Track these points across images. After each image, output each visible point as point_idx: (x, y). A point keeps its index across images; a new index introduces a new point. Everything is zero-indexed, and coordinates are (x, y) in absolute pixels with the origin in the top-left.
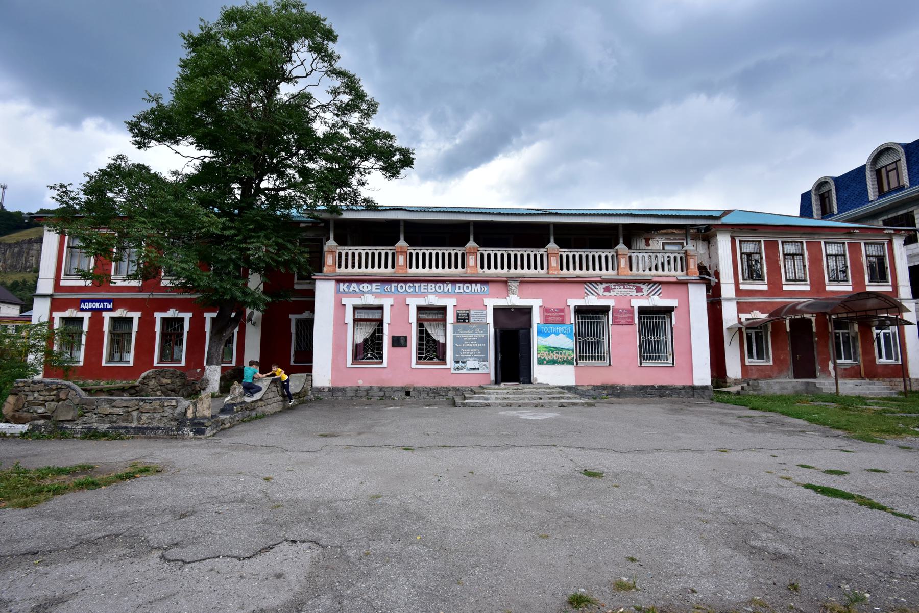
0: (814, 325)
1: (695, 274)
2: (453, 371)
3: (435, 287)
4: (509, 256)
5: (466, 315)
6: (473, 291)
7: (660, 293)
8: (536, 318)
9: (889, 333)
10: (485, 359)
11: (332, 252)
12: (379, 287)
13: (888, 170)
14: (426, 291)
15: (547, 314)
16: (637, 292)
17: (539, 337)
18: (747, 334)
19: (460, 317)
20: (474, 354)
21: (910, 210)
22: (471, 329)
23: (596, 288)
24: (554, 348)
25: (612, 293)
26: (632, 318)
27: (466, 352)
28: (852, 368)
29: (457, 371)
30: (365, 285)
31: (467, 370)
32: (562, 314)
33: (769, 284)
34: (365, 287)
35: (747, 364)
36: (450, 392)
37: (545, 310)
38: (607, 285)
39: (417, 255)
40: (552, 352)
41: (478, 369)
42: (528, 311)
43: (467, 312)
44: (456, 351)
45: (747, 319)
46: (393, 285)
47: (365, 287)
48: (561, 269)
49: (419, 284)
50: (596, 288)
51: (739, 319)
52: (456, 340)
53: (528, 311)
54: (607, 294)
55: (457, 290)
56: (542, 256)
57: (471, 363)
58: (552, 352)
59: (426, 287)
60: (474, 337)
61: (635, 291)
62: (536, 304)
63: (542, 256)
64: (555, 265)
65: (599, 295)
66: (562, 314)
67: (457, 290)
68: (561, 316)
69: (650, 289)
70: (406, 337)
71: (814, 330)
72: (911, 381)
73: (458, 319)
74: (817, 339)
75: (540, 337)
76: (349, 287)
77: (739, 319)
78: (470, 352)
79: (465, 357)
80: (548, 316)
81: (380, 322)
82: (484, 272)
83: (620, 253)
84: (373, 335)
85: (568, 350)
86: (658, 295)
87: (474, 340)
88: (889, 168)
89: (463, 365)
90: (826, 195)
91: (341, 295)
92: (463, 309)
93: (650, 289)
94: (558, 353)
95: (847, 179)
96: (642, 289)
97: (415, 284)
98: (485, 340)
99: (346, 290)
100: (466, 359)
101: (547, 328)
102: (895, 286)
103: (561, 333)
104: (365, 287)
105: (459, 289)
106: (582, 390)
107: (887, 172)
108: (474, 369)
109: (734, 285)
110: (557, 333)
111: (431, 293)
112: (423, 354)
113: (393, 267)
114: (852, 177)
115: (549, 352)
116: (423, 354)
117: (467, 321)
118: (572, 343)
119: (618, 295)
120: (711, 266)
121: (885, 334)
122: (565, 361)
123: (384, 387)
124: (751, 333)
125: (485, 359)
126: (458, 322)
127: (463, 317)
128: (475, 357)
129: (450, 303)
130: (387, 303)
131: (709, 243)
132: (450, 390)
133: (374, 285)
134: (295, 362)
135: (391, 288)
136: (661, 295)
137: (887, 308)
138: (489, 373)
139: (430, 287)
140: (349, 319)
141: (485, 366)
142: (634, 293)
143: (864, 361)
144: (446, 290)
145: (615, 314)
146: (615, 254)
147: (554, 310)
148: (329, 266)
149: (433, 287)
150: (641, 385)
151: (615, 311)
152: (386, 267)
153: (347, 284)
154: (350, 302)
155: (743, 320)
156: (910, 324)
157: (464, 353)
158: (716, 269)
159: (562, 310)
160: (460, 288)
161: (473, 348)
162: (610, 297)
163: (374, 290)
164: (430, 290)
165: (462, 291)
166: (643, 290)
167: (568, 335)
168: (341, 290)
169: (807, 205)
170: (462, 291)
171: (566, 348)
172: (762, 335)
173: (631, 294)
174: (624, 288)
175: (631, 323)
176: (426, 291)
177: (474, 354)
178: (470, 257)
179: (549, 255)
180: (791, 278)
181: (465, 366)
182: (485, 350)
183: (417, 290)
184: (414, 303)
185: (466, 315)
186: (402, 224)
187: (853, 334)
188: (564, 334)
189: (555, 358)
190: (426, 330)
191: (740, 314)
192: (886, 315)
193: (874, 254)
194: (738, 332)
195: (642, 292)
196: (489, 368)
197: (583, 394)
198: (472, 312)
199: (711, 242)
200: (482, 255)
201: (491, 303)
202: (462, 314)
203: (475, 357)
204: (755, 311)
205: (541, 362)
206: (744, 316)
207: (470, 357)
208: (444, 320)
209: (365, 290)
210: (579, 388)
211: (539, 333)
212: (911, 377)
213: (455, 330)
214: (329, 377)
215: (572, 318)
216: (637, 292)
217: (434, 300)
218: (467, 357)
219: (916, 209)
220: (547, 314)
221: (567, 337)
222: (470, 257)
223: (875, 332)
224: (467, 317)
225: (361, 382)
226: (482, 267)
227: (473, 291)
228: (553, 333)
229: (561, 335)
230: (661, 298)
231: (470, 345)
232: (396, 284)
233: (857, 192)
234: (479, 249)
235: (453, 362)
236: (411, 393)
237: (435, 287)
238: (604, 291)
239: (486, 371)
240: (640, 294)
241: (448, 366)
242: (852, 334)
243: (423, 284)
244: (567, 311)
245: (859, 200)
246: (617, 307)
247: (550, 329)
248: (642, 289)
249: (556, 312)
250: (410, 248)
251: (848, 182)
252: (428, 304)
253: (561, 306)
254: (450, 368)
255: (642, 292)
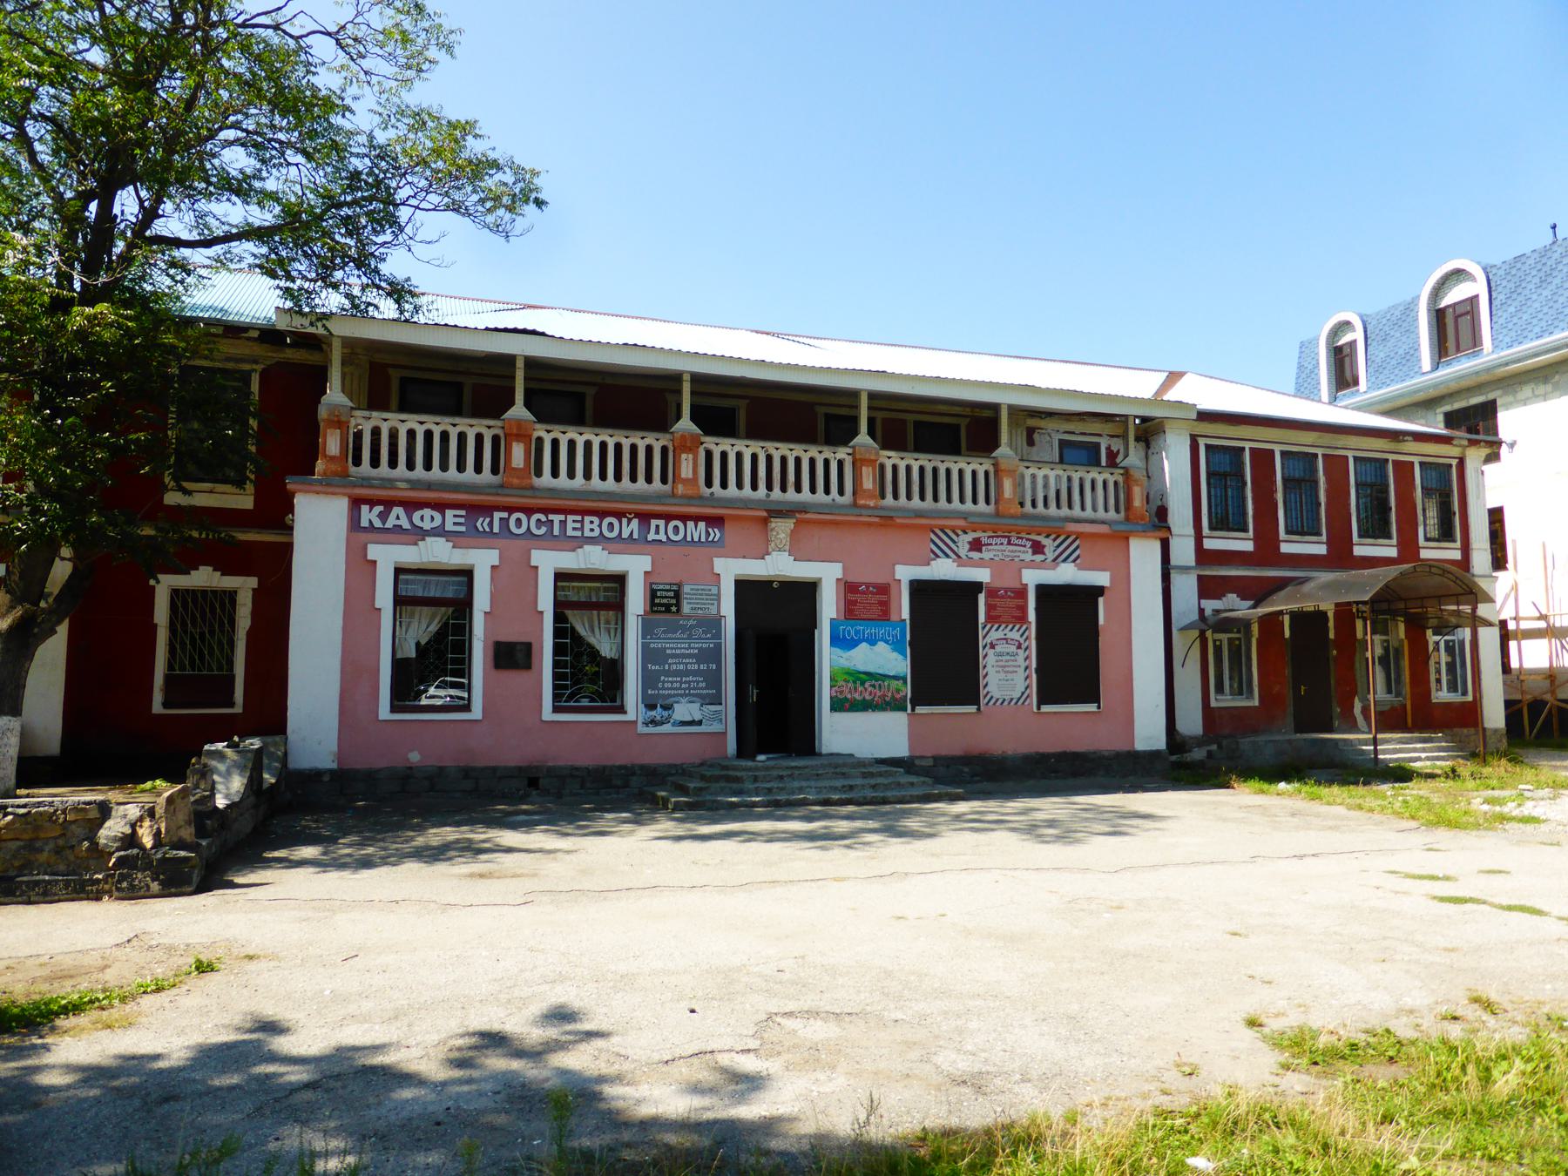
0: (1331, 624)
1: (1142, 519)
2: (641, 729)
3: (600, 526)
4: (769, 458)
5: (672, 594)
6: (689, 539)
7: (1078, 557)
8: (829, 606)
9: (1453, 641)
10: (716, 700)
11: (340, 424)
12: (462, 520)
13: (1458, 313)
14: (579, 534)
15: (851, 597)
16: (1034, 553)
17: (833, 649)
18: (1215, 641)
19: (657, 601)
20: (689, 688)
21: (1491, 396)
22: (684, 629)
23: (954, 542)
24: (865, 673)
25: (986, 555)
26: (1023, 609)
27: (672, 682)
28: (1393, 709)
29: (652, 729)
30: (427, 512)
31: (673, 725)
32: (883, 598)
33: (1256, 539)
34: (427, 518)
35: (1213, 704)
36: (634, 778)
37: (849, 589)
38: (976, 535)
39: (555, 443)
40: (863, 683)
41: (700, 723)
42: (808, 590)
43: (675, 588)
44: (649, 680)
45: (1217, 611)
46: (497, 515)
47: (427, 518)
48: (883, 496)
49: (562, 517)
50: (954, 542)
51: (1201, 611)
52: (648, 655)
53: (808, 590)
54: (975, 555)
55: (651, 536)
56: (841, 463)
57: (684, 711)
58: (863, 683)
59: (578, 525)
60: (689, 648)
61: (1030, 550)
62: (828, 575)
63: (841, 463)
64: (871, 486)
65: (959, 557)
66: (883, 598)
67: (651, 536)
68: (881, 603)
69: (1058, 546)
70: (528, 646)
71: (1332, 635)
72: (1488, 733)
73: (653, 604)
74: (1335, 652)
75: (838, 651)
76: (383, 516)
77: (1201, 611)
78: (681, 682)
79: (670, 696)
80: (855, 603)
81: (463, 606)
82: (712, 494)
83: (1003, 467)
84: (440, 636)
85: (896, 678)
86: (1074, 561)
87: (689, 656)
88: (1460, 310)
89: (666, 714)
90: (1346, 351)
91: (363, 537)
92: (666, 578)
93: (1058, 546)
94: (874, 686)
95: (1384, 321)
96: (1044, 546)
97: (551, 517)
98: (716, 654)
99: (378, 523)
100: (672, 699)
101: (851, 629)
102: (1466, 549)
103: (882, 640)
104: (427, 518)
105: (657, 532)
106: (921, 766)
107: (1456, 318)
108: (692, 723)
109: (1193, 539)
110: (872, 642)
111: (591, 541)
112: (565, 687)
113: (495, 470)
114: (1394, 318)
115: (854, 682)
116: (565, 687)
117: (674, 609)
118: (904, 664)
119: (996, 558)
120: (1151, 496)
121: (1447, 642)
122: (888, 704)
123: (474, 769)
124: (1221, 641)
125: (716, 700)
126: (653, 612)
127: (665, 601)
128: (694, 695)
129: (636, 567)
130: (482, 560)
131: (1148, 446)
132: (634, 774)
133: (449, 513)
134: (165, 705)
135: (491, 524)
136: (1078, 561)
137: (1457, 595)
138: (724, 734)
139: (587, 526)
140: (384, 597)
141: (717, 718)
142: (1028, 556)
143: (1413, 694)
144: (625, 535)
145: (992, 601)
146: (992, 470)
147: (868, 587)
148: (332, 458)
149: (595, 526)
150: (1037, 753)
151: (992, 593)
152: (478, 469)
153: (379, 509)
154: (387, 556)
155: (1208, 612)
156: (1490, 624)
157: (668, 684)
158: (1160, 503)
159: (884, 590)
160: (659, 530)
161: (687, 673)
162: (981, 564)
163: (449, 527)
164: (587, 533)
165: (664, 539)
166: (1046, 550)
167: (897, 646)
168: (364, 523)
169: (1310, 367)
170: (664, 539)
171: (892, 674)
172: (1240, 645)
173: (1023, 556)
174: (1009, 543)
175: (1022, 619)
176: (579, 534)
177: (689, 688)
178: (684, 456)
179: (858, 464)
180: (1295, 529)
181: (670, 716)
182: (715, 680)
183: (556, 531)
184: (548, 562)
185: (672, 594)
186: (520, 364)
187: (1396, 644)
188: (887, 642)
189: (868, 697)
190: (573, 629)
191: (1203, 601)
192: (1455, 608)
193: (1434, 486)
194: (1198, 640)
195: (1044, 553)
196: (724, 720)
197: (925, 772)
198: (686, 589)
199: (1153, 444)
200: (709, 454)
201: (730, 569)
202: (664, 593)
203: (694, 695)
204: (1230, 595)
205: (838, 705)
206: (1210, 605)
207: (681, 695)
208: (618, 606)
209: (427, 525)
210: (917, 762)
211: (836, 640)
212: (1487, 725)
213: (647, 629)
214: (333, 746)
215: (903, 608)
216: (1034, 553)
217: (594, 559)
218: (674, 695)
219: (1501, 397)
220: (851, 597)
221: (895, 650)
222: (684, 456)
223: (1432, 638)
224: (674, 601)
225: (414, 757)
226: (709, 484)
227: (689, 539)
228: (864, 640)
229: (881, 645)
230: (1081, 568)
231: (681, 667)
232: (505, 515)
233: (1401, 351)
234: (704, 439)
235: (641, 706)
236: (541, 781)
237: (600, 526)
238: (970, 550)
239: (716, 727)
240: (1039, 558)
241: (631, 716)
242: (1394, 643)
243: (570, 518)
244: (893, 592)
245: (1405, 369)
246: (998, 584)
247: (857, 632)
248: (1044, 546)
249: (872, 593)
250: (538, 426)
251: (1386, 328)
252: (583, 566)
253: (881, 580)
254: (635, 722)
255: (1044, 553)
